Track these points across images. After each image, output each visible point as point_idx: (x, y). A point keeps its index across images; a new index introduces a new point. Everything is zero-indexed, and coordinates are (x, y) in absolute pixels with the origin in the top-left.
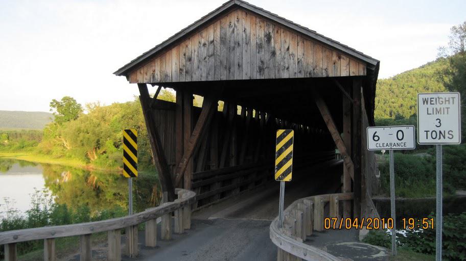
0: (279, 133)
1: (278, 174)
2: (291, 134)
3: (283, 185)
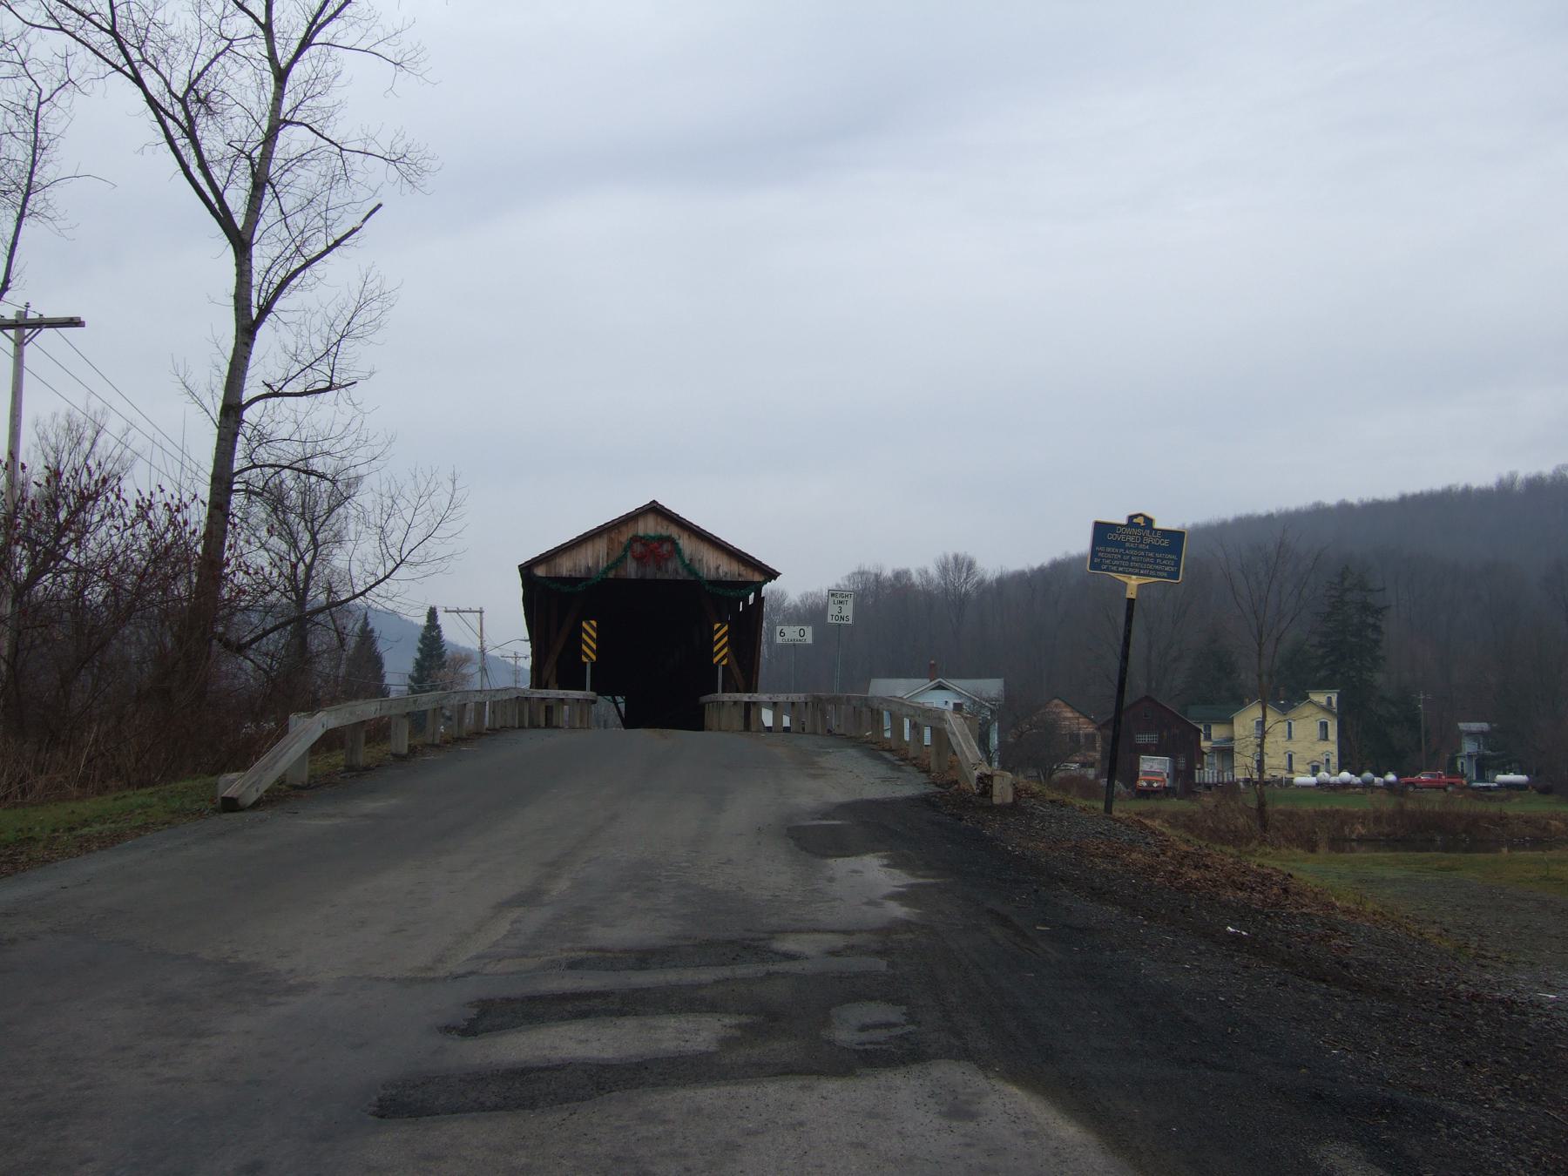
0: (717, 626)
1: (716, 660)
2: (726, 628)
3: (720, 669)
